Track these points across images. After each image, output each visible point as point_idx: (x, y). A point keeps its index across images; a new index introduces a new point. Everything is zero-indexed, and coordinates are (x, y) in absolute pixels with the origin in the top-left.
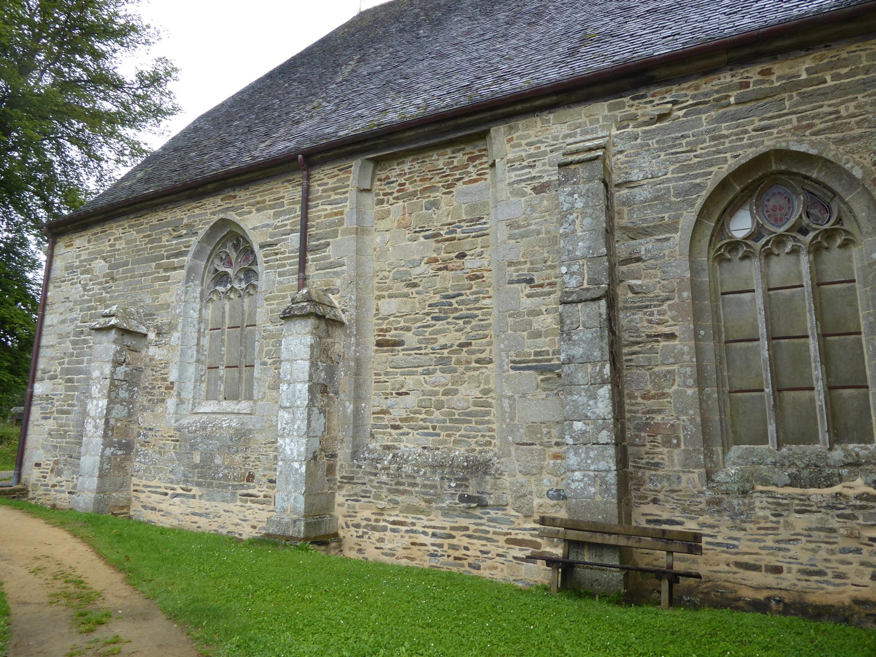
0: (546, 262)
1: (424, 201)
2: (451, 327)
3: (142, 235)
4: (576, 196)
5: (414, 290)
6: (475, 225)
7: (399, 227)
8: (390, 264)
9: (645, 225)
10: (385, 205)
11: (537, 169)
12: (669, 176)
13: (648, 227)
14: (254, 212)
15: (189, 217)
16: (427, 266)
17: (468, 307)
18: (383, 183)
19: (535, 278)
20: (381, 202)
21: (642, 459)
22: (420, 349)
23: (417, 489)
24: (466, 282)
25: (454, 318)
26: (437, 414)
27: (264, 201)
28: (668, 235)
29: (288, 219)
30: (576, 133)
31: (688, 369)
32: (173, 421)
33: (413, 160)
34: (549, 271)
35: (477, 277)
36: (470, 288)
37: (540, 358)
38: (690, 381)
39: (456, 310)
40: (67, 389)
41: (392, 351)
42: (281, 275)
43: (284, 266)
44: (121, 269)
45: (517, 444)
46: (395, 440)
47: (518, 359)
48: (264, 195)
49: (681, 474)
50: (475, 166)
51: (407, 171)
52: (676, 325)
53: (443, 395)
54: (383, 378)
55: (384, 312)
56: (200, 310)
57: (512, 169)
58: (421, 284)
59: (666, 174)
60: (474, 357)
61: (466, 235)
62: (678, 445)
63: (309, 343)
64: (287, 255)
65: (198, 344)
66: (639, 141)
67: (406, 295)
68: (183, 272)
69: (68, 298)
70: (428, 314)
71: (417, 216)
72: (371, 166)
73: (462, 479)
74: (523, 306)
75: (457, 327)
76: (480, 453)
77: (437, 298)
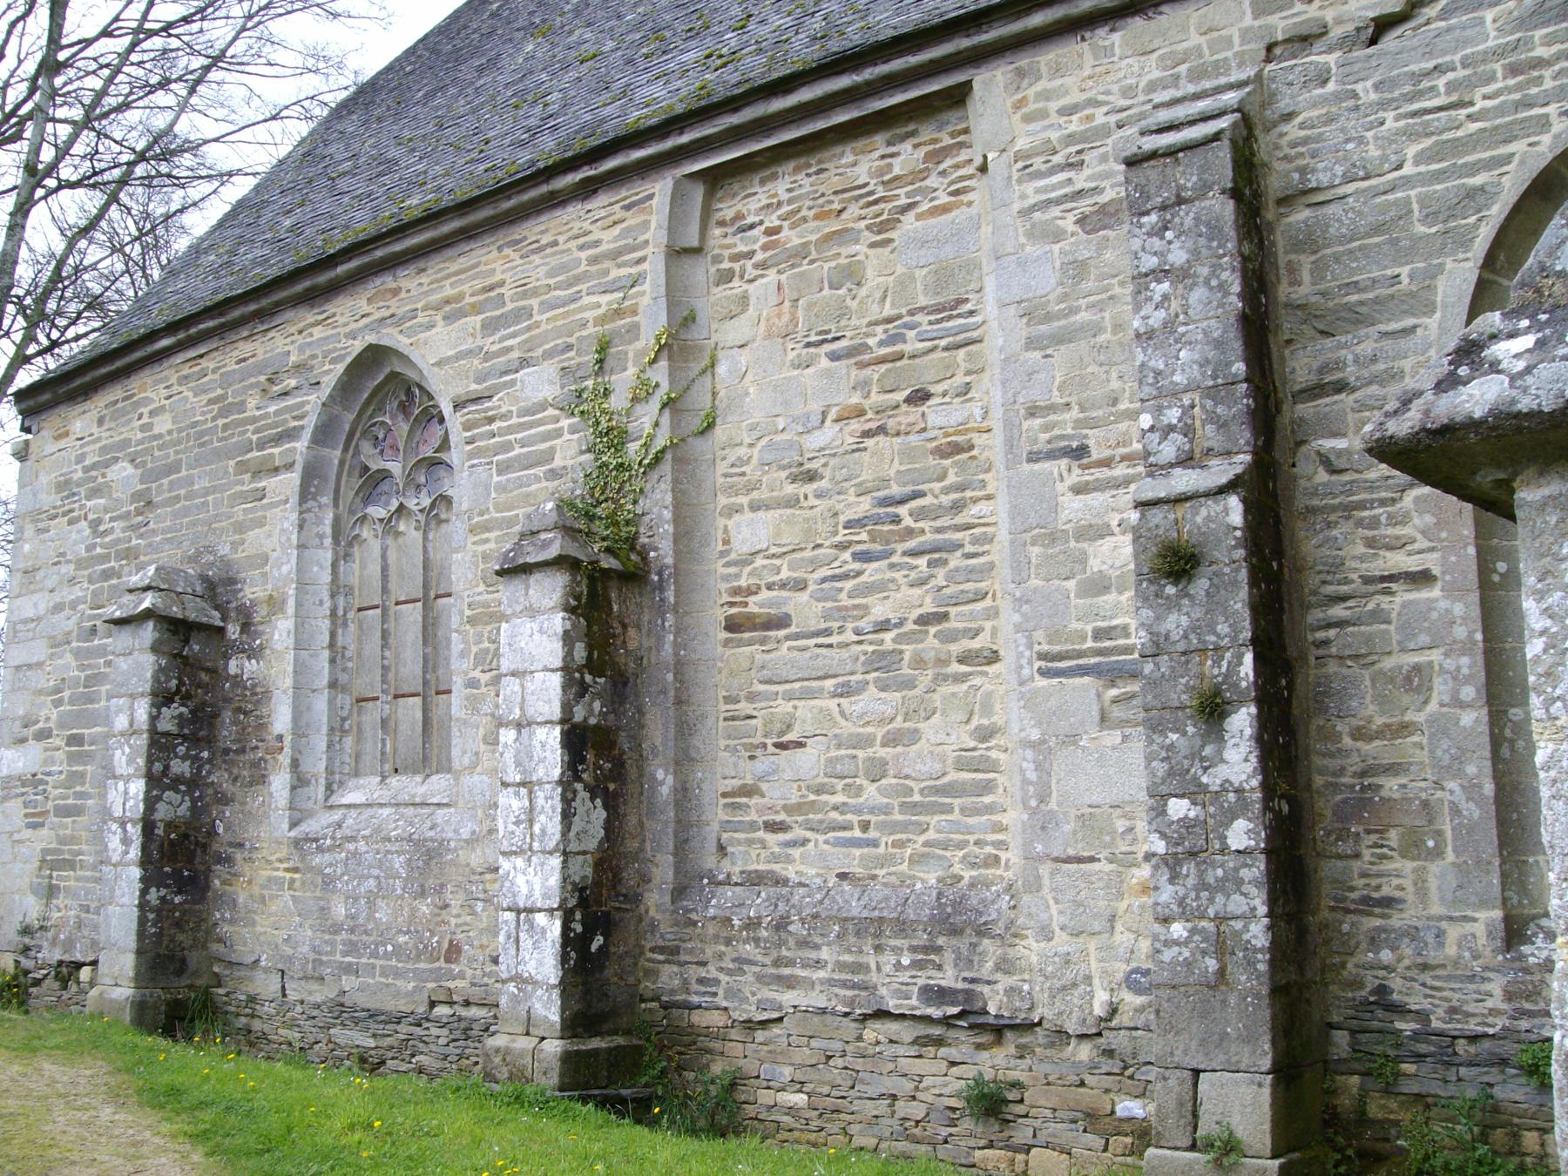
0: (1115, 402)
1: (826, 266)
2: (898, 575)
3: (205, 398)
4: (1169, 235)
5: (809, 488)
6: (950, 318)
7: (769, 336)
8: (752, 428)
9: (1354, 298)
10: (736, 283)
11: (1087, 172)
12: (1408, 169)
13: (1361, 303)
14: (441, 323)
15: (301, 349)
16: (837, 427)
17: (938, 523)
18: (730, 230)
19: (1091, 443)
20: (727, 277)
21: (1352, 889)
22: (827, 632)
23: (822, 974)
24: (932, 461)
25: (904, 554)
26: (871, 790)
27: (460, 297)
28: (1410, 322)
29: (513, 335)
30: (1177, 77)
31: (1465, 660)
32: (285, 826)
33: (797, 170)
34: (1123, 426)
35: (957, 449)
36: (941, 478)
37: (1108, 644)
38: (1468, 692)
39: (910, 533)
40: (72, 758)
41: (763, 642)
42: (503, 469)
43: (507, 447)
44: (165, 481)
45: (1056, 860)
46: (775, 859)
47: (1057, 648)
48: (461, 282)
49: (1444, 925)
50: (943, 173)
51: (785, 196)
52: (1432, 549)
53: (884, 745)
54: (744, 707)
55: (740, 547)
56: (334, 566)
57: (1028, 173)
58: (827, 473)
59: (1399, 167)
60: (956, 648)
61: (928, 344)
62: (1438, 853)
63: (560, 630)
64: (514, 420)
65: (332, 645)
66: (1331, 86)
67: (792, 502)
68: (293, 478)
69: (62, 555)
70: (842, 547)
71: (810, 306)
72: (698, 192)
73: (926, 949)
74: (1063, 516)
75: (913, 575)
76: (972, 885)
77: (864, 506)
